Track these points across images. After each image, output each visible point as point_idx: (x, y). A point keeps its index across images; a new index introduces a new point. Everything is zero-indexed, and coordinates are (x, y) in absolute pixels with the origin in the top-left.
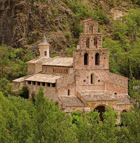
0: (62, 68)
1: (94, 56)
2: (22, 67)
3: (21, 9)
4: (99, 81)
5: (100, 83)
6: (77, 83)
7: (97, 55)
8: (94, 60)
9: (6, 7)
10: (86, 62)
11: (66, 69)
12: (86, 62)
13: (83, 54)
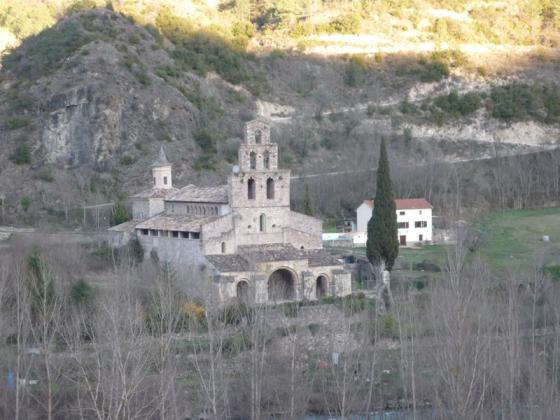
0: (205, 205)
1: (264, 183)
2: (394, 153)
3: (108, 103)
4: (274, 226)
5: (277, 230)
6: (237, 231)
7: (270, 181)
8: (264, 190)
9: (79, 99)
10: (251, 195)
11: (213, 206)
12: (251, 195)
13: (246, 180)
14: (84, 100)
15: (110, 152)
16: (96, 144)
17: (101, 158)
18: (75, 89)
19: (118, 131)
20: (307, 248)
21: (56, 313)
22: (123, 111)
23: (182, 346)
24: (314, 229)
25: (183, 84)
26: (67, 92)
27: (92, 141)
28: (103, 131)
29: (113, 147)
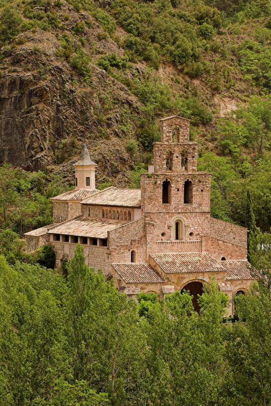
0: (119, 209)
1: (181, 185)
3: (41, 96)
4: (191, 234)
5: (194, 239)
6: (149, 237)
7: (188, 185)
8: (181, 194)
9: (11, 91)
10: (166, 199)
11: (127, 211)
12: (166, 199)
13: (160, 182)
21: (234, 198)
23: (136, 307)
25: (129, 76)
27: (23, 137)
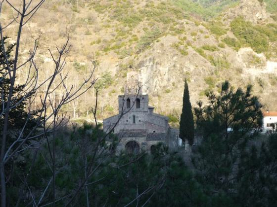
3: (161, 64)
5: (141, 123)
14: (151, 63)
15: (160, 87)
16: (154, 84)
17: (156, 90)
18: (148, 58)
19: (166, 77)
20: (156, 132)
22: (169, 68)
24: (161, 123)
26: (145, 59)
28: (158, 77)
29: (162, 85)
